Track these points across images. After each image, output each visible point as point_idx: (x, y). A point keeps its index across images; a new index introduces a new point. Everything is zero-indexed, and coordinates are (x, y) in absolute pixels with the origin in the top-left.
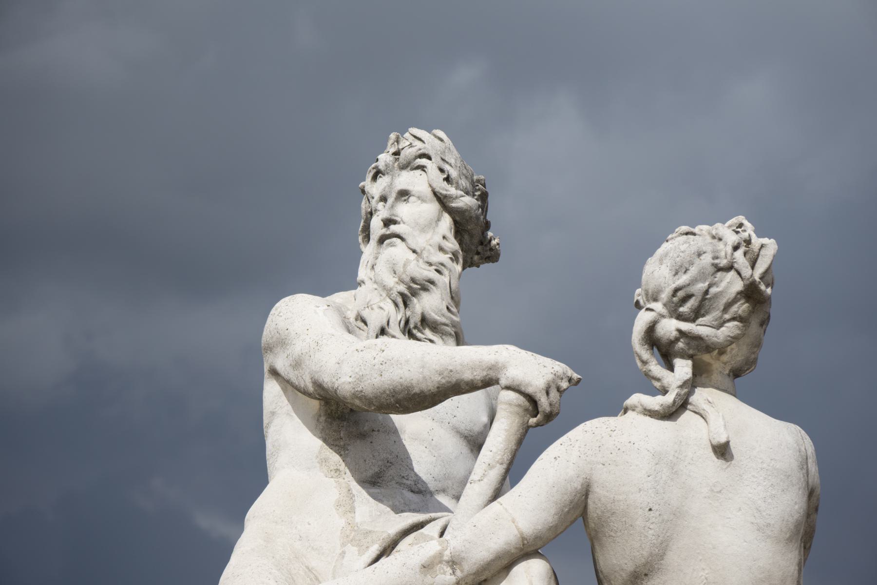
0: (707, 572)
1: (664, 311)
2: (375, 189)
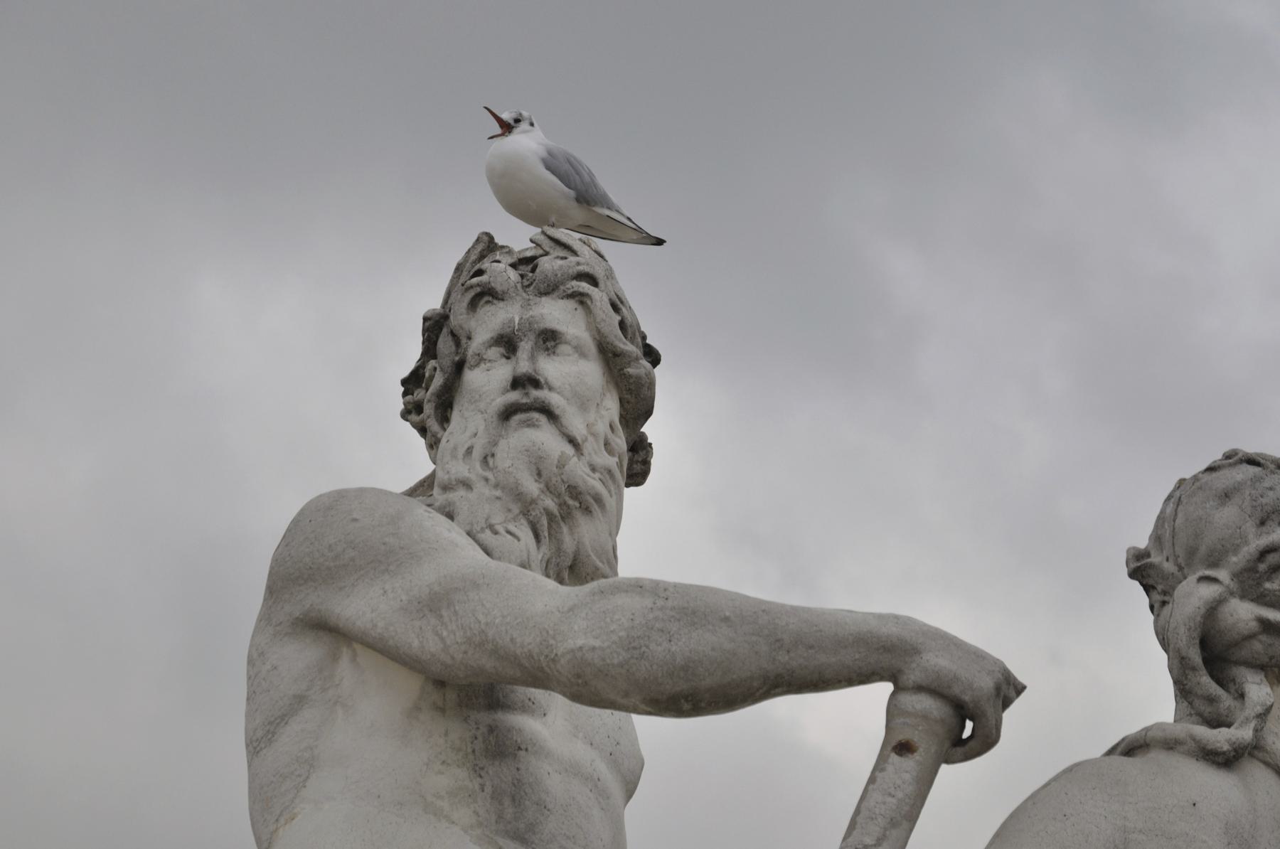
1: (1234, 586)
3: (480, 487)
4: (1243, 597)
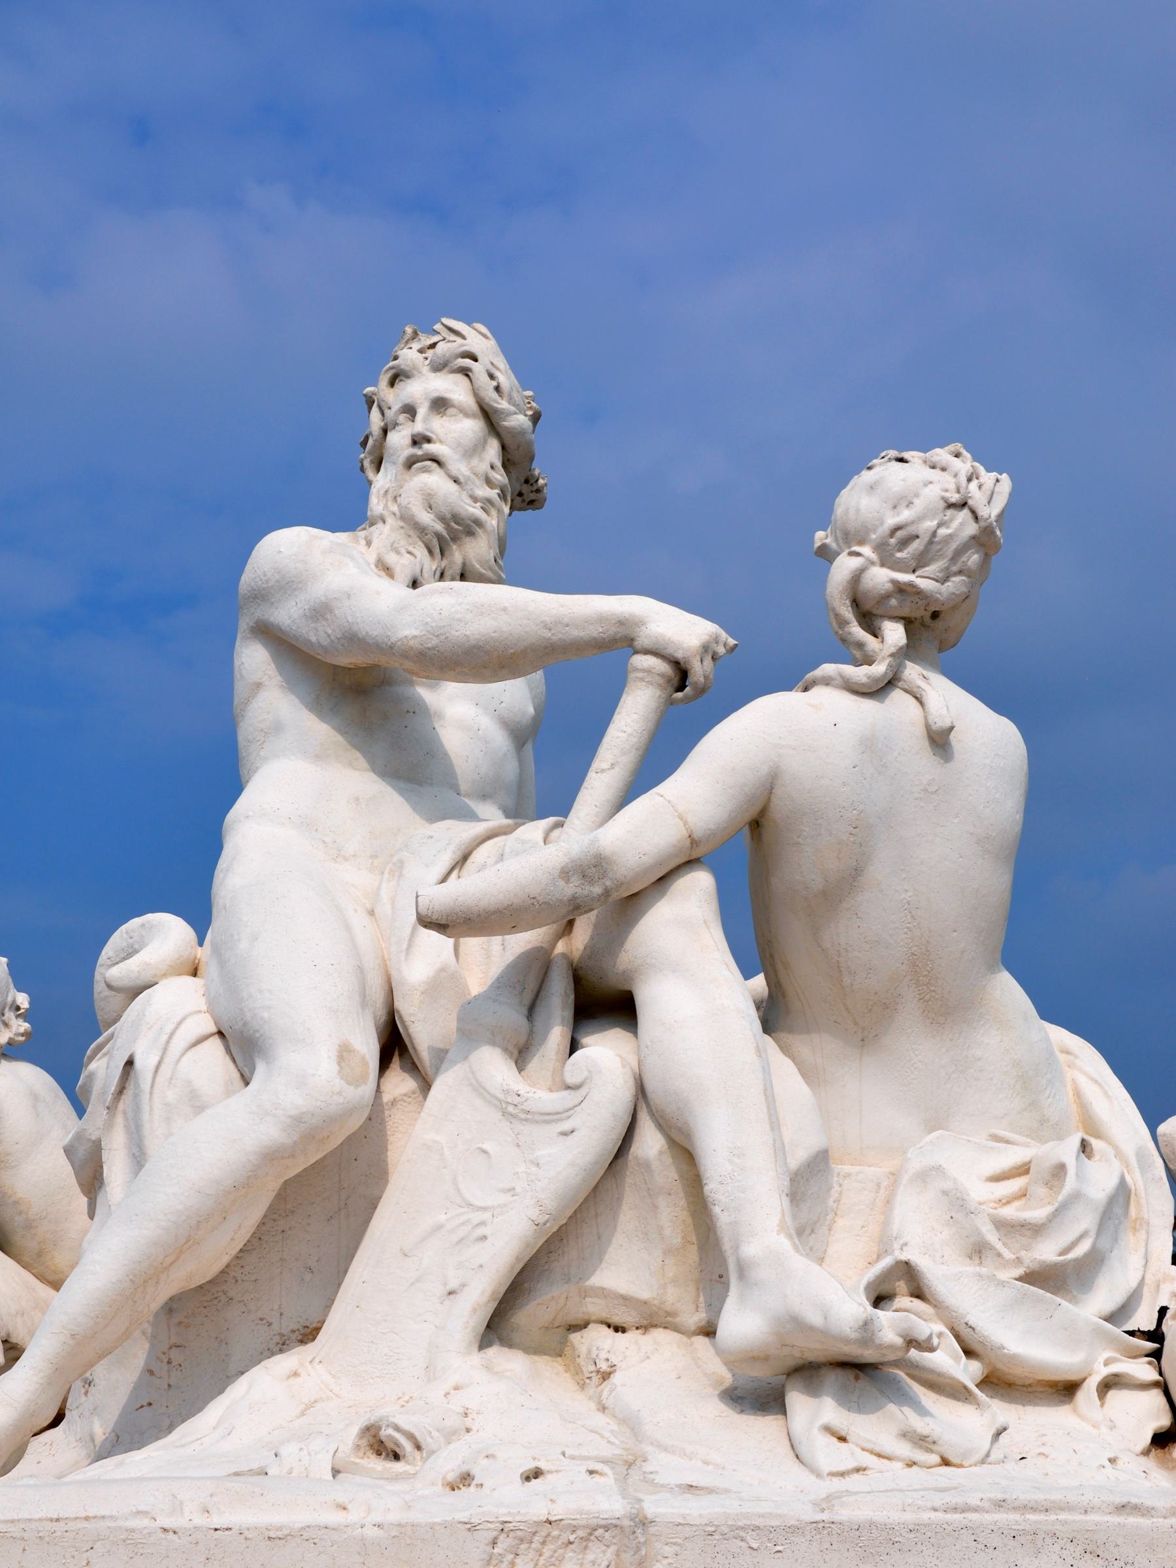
0: (910, 894)
1: (874, 557)
2: (394, 398)
3: (390, 521)
4: (883, 565)
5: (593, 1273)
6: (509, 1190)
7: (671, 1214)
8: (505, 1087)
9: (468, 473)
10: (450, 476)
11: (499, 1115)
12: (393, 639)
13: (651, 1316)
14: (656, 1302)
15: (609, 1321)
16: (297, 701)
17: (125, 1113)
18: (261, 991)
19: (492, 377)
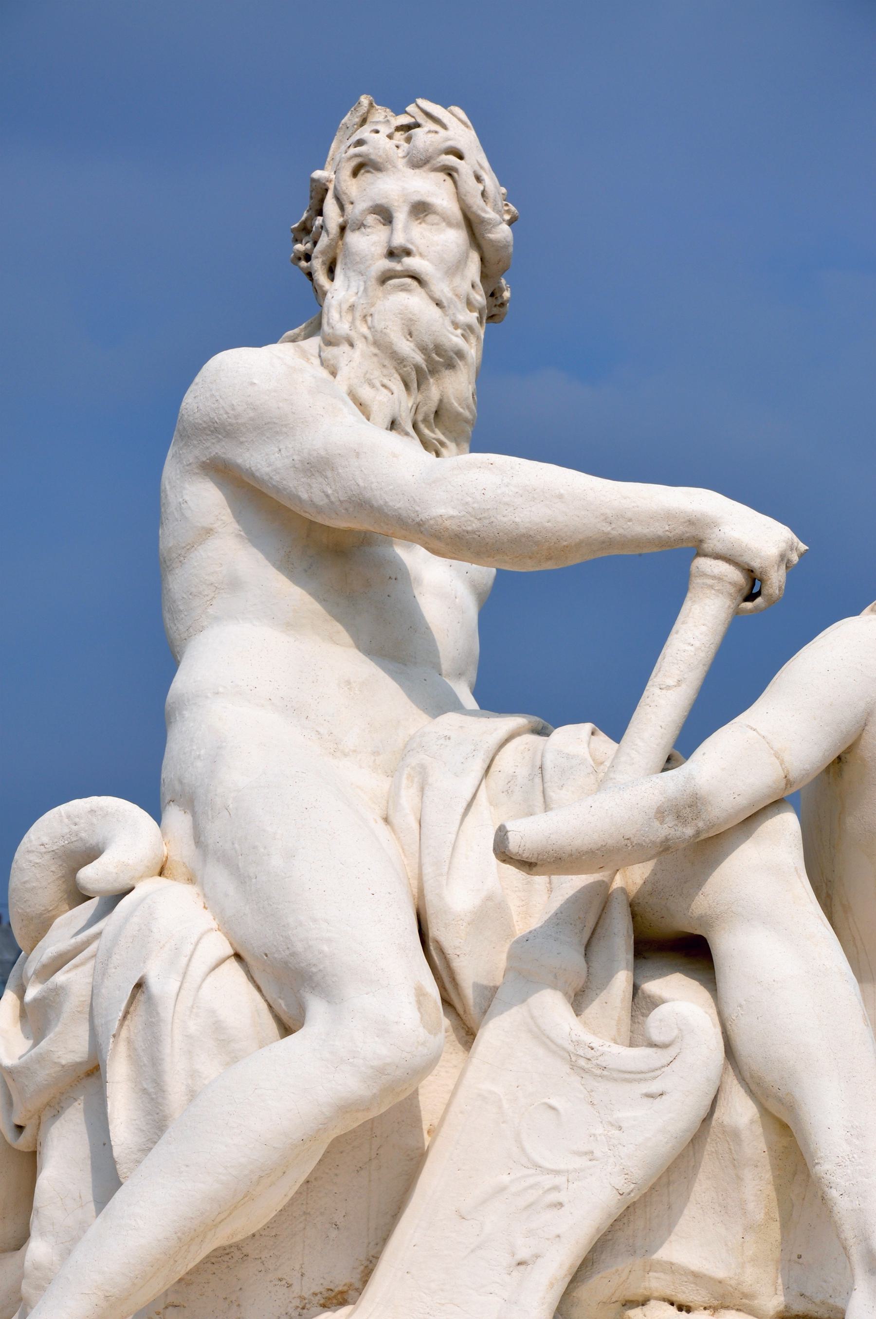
2: (363, 192)
3: (360, 345)
5: (666, 1245)
6: (586, 1153)
7: (757, 1187)
8: (574, 1038)
9: (450, 295)
10: (432, 298)
11: (566, 1068)
12: (424, 516)
13: (723, 1296)
14: (733, 1282)
15: (674, 1299)
16: (260, 556)
17: (129, 1042)
18: (315, 921)
19: (478, 179)
